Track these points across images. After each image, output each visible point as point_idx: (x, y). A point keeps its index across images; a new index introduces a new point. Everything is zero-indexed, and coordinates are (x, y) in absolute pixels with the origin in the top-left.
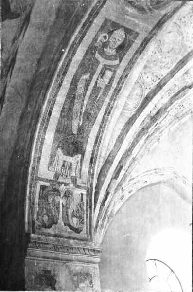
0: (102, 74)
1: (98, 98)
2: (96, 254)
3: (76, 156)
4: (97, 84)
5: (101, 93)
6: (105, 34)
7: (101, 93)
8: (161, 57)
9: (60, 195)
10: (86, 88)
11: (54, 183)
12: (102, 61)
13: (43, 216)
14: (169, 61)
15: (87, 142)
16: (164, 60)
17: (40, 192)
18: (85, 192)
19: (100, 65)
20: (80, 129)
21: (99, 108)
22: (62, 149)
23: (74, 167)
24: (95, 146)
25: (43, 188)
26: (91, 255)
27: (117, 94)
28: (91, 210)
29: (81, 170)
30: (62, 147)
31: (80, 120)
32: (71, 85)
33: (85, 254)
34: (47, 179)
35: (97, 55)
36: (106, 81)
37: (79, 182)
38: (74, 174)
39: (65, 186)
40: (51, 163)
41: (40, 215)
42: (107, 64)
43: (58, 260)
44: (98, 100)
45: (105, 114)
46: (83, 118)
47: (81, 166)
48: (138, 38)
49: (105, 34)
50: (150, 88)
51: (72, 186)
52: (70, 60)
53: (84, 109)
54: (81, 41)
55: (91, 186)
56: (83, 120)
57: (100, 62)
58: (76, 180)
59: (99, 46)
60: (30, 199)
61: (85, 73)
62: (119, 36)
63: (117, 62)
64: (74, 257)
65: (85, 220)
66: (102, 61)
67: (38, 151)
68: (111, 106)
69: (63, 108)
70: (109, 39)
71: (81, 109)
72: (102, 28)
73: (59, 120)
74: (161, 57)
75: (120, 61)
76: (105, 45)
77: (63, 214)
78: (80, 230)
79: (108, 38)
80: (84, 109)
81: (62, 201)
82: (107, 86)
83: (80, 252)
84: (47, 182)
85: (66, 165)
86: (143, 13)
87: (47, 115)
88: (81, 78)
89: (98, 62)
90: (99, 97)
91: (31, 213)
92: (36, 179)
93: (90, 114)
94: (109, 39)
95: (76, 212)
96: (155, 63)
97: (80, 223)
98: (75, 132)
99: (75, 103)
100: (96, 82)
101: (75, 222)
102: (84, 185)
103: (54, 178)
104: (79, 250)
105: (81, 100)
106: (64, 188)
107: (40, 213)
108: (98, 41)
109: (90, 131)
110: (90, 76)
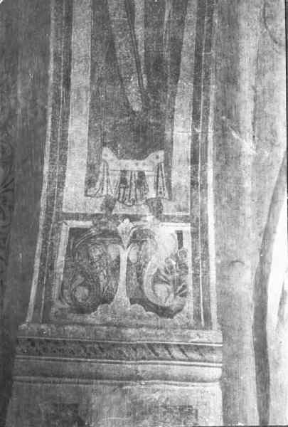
2: (207, 357)
3: (152, 156)
9: (120, 242)
11: (103, 220)
17: (69, 242)
18: (187, 228)
22: (114, 149)
25: (75, 233)
26: (191, 360)
29: (169, 182)
31: (140, 78)
33: (173, 358)
34: (85, 215)
39: (131, 221)
40: (90, 183)
41: (67, 288)
43: (100, 379)
46: (147, 72)
51: (150, 218)
56: (149, 78)
60: (43, 259)
64: (140, 368)
65: (190, 288)
71: (135, 53)
77: (128, 279)
80: (142, 52)
81: (127, 254)
83: (157, 354)
84: (89, 220)
85: (128, 178)
91: (45, 283)
92: (58, 219)
95: (166, 272)
101: (163, 295)
103: (102, 209)
104: (153, 351)
106: (131, 225)
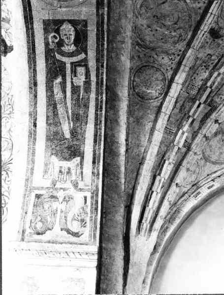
1: (81, 97)
3: (74, 160)
5: (82, 91)
6: (53, 34)
7: (82, 91)
10: (64, 92)
12: (68, 61)
13: (36, 224)
14: (181, 34)
15: (84, 144)
16: (173, 34)
18: (89, 195)
19: (67, 65)
20: (73, 133)
21: (86, 106)
23: (73, 172)
24: (94, 146)
28: (97, 212)
30: (55, 153)
32: (47, 93)
33: (76, 258)
35: (58, 57)
37: (81, 185)
38: (74, 178)
40: (46, 172)
42: (72, 61)
44: (82, 98)
45: (96, 110)
46: (73, 120)
47: (82, 168)
48: (88, 25)
49: (53, 34)
50: (172, 69)
53: (70, 112)
55: (97, 187)
58: (77, 183)
61: (56, 77)
66: (68, 61)
67: (31, 162)
68: (100, 101)
69: (48, 117)
72: (46, 31)
73: (47, 129)
76: (60, 44)
78: (80, 234)
79: (58, 37)
80: (70, 112)
82: (85, 83)
87: (32, 127)
88: (54, 84)
90: (81, 94)
93: (78, 115)
96: (163, 40)
97: (81, 226)
99: (58, 108)
100: (72, 83)
102: (87, 187)
105: (64, 104)
107: (33, 221)
108: (51, 44)
109: (85, 131)
110: (63, 79)
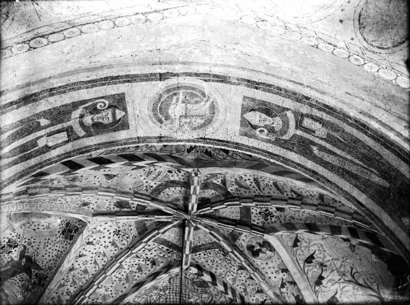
0: (307, 130)
4: (323, 137)
8: (185, 125)
12: (292, 131)
27: (335, 111)
36: (316, 126)
52: (299, 165)
53: (357, 161)
54: (273, 154)
56: (372, 167)
57: (294, 134)
59: (273, 136)
61: (311, 152)
62: (255, 118)
63: (289, 114)
70: (261, 127)
71: (358, 165)
74: (185, 125)
75: (288, 109)
76: (271, 130)
86: (216, 102)
89: (294, 136)
94: (261, 127)
98: (387, 184)
100: (322, 139)
109: (388, 162)
